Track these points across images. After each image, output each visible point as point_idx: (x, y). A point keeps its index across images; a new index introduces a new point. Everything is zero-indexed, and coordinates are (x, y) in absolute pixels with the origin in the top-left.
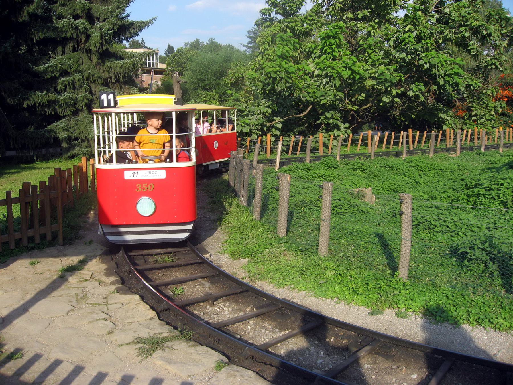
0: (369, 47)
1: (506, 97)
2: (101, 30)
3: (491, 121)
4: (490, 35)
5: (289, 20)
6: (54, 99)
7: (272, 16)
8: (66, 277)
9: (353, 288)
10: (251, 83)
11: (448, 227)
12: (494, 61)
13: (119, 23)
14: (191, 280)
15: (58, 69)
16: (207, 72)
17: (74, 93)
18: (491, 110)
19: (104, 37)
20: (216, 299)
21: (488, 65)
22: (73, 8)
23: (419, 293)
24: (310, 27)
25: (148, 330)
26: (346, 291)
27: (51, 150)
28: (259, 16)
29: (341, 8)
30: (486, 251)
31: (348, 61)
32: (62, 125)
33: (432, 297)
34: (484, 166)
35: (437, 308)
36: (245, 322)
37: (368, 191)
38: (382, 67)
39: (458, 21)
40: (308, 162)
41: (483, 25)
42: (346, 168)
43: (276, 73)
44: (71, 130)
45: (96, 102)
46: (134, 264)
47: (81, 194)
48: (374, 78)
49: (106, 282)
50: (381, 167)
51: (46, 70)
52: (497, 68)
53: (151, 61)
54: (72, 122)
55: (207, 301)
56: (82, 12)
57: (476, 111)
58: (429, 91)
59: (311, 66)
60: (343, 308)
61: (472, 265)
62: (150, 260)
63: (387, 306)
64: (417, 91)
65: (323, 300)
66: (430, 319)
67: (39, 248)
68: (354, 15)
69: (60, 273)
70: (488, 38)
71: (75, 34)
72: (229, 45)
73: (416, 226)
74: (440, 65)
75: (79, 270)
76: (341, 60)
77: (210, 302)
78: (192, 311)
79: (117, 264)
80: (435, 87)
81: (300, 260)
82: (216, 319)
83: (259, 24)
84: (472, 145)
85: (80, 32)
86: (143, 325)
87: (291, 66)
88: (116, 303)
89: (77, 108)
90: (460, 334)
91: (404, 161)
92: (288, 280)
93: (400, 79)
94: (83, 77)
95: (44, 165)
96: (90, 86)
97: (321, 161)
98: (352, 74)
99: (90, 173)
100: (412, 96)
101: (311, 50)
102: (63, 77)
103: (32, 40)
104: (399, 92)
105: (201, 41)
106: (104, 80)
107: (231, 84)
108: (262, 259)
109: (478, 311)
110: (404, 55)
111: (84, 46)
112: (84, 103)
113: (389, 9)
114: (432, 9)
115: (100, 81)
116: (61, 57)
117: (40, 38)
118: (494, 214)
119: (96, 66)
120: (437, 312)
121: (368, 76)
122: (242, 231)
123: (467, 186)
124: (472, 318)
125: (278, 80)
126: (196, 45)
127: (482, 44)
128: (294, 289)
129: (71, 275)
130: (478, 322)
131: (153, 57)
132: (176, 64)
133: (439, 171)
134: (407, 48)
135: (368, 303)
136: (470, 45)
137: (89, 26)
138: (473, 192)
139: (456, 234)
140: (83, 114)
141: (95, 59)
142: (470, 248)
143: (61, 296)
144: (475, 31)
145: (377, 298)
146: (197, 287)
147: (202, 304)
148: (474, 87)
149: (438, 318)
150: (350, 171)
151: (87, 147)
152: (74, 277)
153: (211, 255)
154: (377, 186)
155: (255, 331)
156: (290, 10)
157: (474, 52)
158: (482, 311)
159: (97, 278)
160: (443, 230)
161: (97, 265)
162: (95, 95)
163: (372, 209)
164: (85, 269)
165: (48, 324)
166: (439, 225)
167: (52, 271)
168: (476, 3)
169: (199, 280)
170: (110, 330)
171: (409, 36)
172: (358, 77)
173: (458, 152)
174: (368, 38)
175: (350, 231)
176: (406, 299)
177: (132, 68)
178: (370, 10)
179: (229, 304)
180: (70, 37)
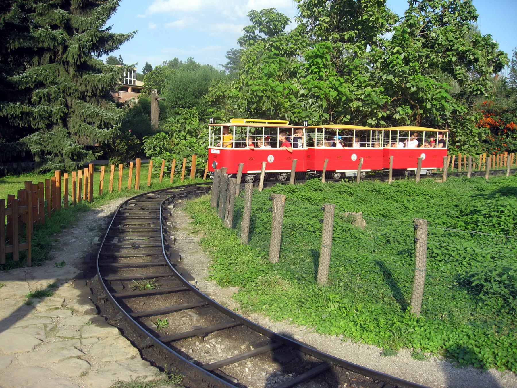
0: (356, 67)
1: (489, 124)
2: (80, 41)
3: (475, 148)
4: (477, 60)
5: (274, 39)
6: (28, 111)
7: (256, 34)
8: (34, 304)
9: (361, 325)
10: (233, 102)
11: (451, 255)
12: (479, 87)
13: (99, 35)
14: (176, 311)
15: (33, 80)
16: (186, 90)
17: (49, 105)
18: (475, 136)
19: (83, 48)
20: (207, 335)
21: (473, 91)
22: (52, 18)
23: (436, 330)
24: (295, 47)
25: (130, 372)
26: (352, 327)
27: (23, 164)
28: (243, 34)
29: (327, 28)
30: (504, 284)
31: (335, 82)
32: (35, 138)
33: (451, 336)
34: (473, 193)
35: (458, 349)
36: (241, 362)
37: (359, 216)
38: (369, 89)
39: (445, 45)
40: (293, 183)
41: (470, 49)
42: (332, 190)
43: (262, 91)
44: (45, 144)
45: (72, 115)
46: (112, 291)
47: (54, 211)
48: (359, 100)
49: (80, 310)
50: (368, 191)
51: (21, 81)
52: (482, 93)
53: (129, 79)
54: (46, 136)
55: (196, 337)
56: (61, 22)
57: (460, 137)
58: (415, 115)
59: (295, 85)
60: (351, 347)
61: (489, 299)
62: (129, 287)
63: (401, 345)
64: (403, 114)
65: (327, 337)
66: (451, 362)
67: (4, 269)
68: (340, 36)
69: (27, 299)
70: (475, 64)
71: (52, 45)
72: (208, 65)
73: (431, 256)
74: (427, 89)
75: (48, 296)
76: (328, 81)
77: (200, 338)
78: (179, 348)
79: (91, 289)
80: (422, 111)
81: (297, 290)
82: (208, 358)
83: (242, 42)
84: (456, 171)
85: (57, 42)
86: (124, 366)
87: (278, 85)
88: (91, 337)
89: (51, 122)
90: (490, 381)
91: (391, 185)
92: (286, 313)
93: (387, 102)
94: (59, 89)
95: (15, 179)
96: (66, 99)
97: (306, 183)
98: (338, 95)
99: (63, 189)
100: (399, 119)
101: (296, 69)
102: (38, 88)
103: (7, 49)
104: (385, 115)
105: (179, 60)
106: (81, 93)
107: (212, 102)
108: (255, 288)
109: (505, 354)
110: (391, 77)
111: (62, 58)
112: (59, 117)
113: (376, 31)
114: (417, 33)
115: (76, 94)
116: (36, 68)
117: (15, 48)
118: (495, 243)
119: (74, 78)
120: (458, 354)
121: (354, 97)
122: (229, 255)
123: (462, 214)
124: (499, 361)
125: (264, 98)
126: (174, 64)
127: (468, 69)
128: (293, 322)
129: (40, 302)
130: (507, 366)
131: (131, 74)
132: (153, 82)
133: (427, 197)
134: (395, 70)
135: (380, 341)
136: (456, 70)
137: (68, 37)
138: (471, 219)
139: (459, 264)
140: (57, 127)
141: (72, 71)
142: (486, 280)
143: (27, 327)
144: (462, 57)
145: (390, 336)
146: (184, 319)
147: (190, 340)
148: (460, 113)
149: (461, 361)
150: (336, 194)
151: (60, 162)
152: (43, 304)
153: (196, 282)
154: (365, 211)
155: (253, 373)
156: (274, 29)
157: (460, 77)
158: (510, 353)
159: (69, 306)
160: (446, 259)
161: (69, 291)
162: (71, 108)
163: (363, 234)
164: (55, 295)
165: (10, 362)
166: (441, 254)
167: (18, 297)
168: (463, 29)
169: (186, 311)
170: (85, 371)
171: (397, 58)
172: (344, 98)
173: (445, 178)
174: (354, 59)
175: (347, 257)
176: (421, 337)
177: (110, 83)
178: (356, 32)
179: (221, 339)
180: (47, 47)
